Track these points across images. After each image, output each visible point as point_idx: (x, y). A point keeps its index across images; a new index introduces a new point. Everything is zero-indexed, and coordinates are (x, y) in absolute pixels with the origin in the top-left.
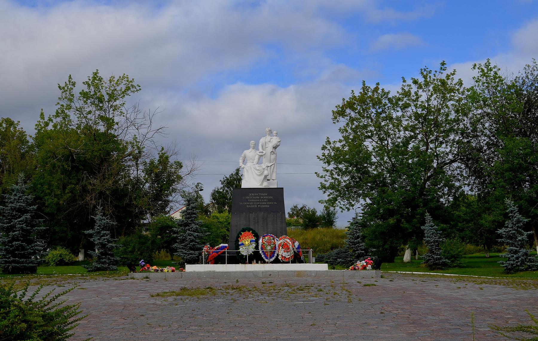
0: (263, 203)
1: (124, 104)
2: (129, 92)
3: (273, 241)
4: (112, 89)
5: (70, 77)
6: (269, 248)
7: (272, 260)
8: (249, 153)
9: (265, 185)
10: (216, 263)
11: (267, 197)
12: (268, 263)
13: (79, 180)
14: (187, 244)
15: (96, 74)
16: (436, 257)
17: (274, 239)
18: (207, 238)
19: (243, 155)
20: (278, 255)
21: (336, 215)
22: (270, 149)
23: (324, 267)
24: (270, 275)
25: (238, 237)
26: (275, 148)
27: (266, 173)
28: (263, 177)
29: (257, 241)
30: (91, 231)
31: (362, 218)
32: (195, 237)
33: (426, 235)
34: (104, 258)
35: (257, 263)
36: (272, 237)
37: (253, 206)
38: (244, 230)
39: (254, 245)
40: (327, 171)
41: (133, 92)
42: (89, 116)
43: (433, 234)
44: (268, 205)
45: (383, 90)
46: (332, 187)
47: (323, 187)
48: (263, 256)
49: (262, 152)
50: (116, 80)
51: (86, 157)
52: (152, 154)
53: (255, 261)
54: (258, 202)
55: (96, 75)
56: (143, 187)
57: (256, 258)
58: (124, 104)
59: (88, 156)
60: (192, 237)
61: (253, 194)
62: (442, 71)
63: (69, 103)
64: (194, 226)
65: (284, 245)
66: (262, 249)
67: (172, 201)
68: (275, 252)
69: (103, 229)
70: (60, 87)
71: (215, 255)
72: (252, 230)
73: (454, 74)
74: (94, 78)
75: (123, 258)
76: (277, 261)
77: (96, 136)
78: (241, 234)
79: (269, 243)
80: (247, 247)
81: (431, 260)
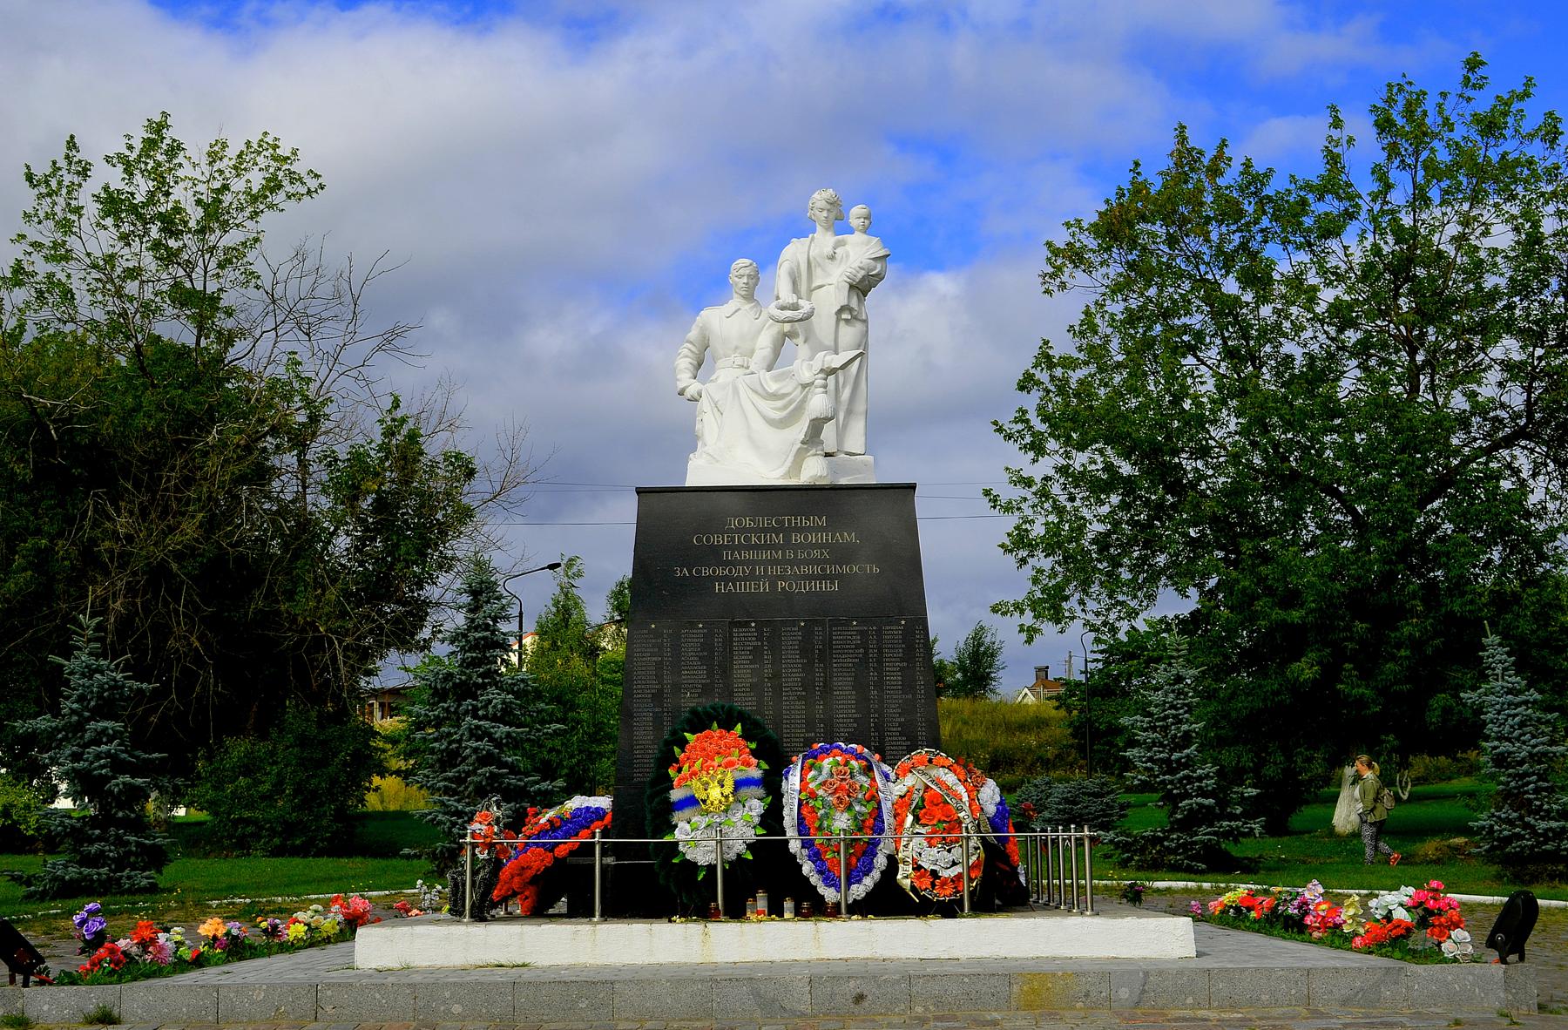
0: (805, 570)
1: (256, 240)
2: (279, 197)
3: (863, 780)
4: (217, 185)
5: (72, 144)
6: (841, 822)
7: (859, 891)
8: (725, 320)
9: (813, 471)
10: (539, 911)
11: (823, 537)
12: (833, 912)
13: (70, 520)
14: (468, 774)
15: (159, 127)
16: (1543, 825)
17: (867, 770)
18: (557, 743)
19: (693, 334)
20: (893, 862)
21: (1000, 659)
22: (831, 294)
23: (1158, 938)
24: (860, 998)
25: (668, 759)
26: (862, 287)
27: (818, 403)
28: (800, 430)
29: (772, 785)
30: (43, 723)
31: (1100, 666)
32: (498, 744)
33: (1491, 729)
34: (99, 839)
35: (776, 910)
36: (859, 757)
37: (751, 587)
38: (699, 723)
39: (756, 807)
40: (1028, 482)
41: (298, 197)
42: (131, 287)
43: (1522, 725)
44: (831, 578)
45: (1247, 165)
46: (1052, 543)
47: (1020, 541)
48: (807, 868)
49: (795, 307)
50: (232, 152)
51: (97, 432)
52: (354, 426)
53: (762, 902)
54: (775, 562)
55: (158, 132)
56: (325, 548)
57: (767, 879)
58: (256, 240)
59: (106, 427)
60: (484, 744)
61: (747, 522)
62: (1470, 93)
63: (59, 236)
64: (496, 697)
65: (929, 803)
66: (802, 827)
67: (438, 604)
68: (875, 843)
69: (101, 712)
70: (29, 177)
71: (538, 860)
72: (742, 717)
73: (1526, 95)
74: (150, 145)
75: (241, 820)
76: (888, 901)
77: (157, 360)
78: (683, 743)
79: (845, 796)
80: (714, 817)
81: (1519, 837)
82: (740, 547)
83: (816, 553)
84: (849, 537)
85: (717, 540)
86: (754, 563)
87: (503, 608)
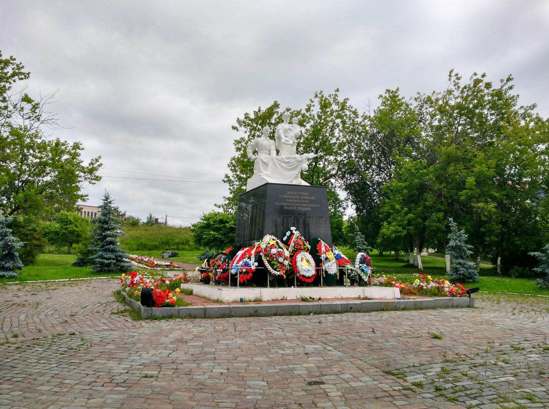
82: (290, 199)
83: (306, 201)
84: (313, 198)
85: (285, 196)
86: (293, 203)
87: (479, 88)
